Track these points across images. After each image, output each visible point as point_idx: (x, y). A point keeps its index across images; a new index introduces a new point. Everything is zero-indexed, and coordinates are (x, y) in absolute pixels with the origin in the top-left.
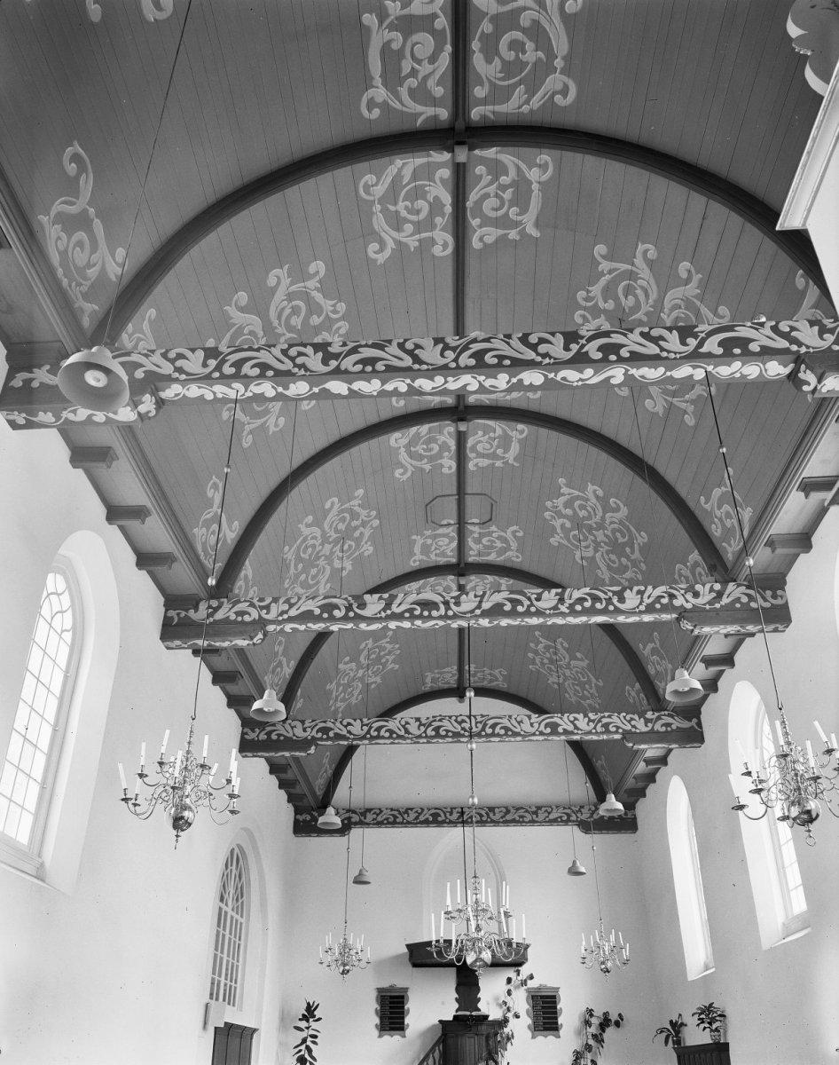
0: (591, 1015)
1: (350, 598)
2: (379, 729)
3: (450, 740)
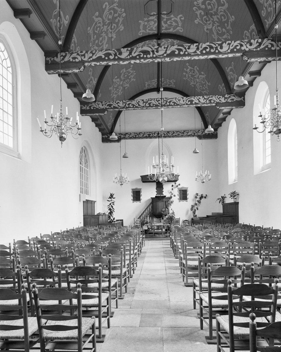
0: (197, 195)
2: (129, 104)
3: (154, 108)
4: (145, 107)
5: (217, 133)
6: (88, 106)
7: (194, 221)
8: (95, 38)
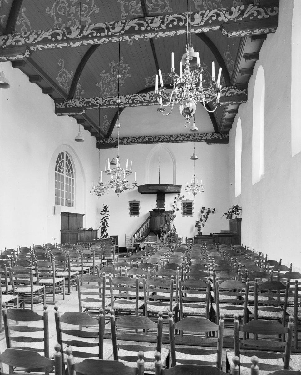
0: (204, 209)
1: (64, 29)
2: (109, 101)
3: (139, 105)
4: (128, 104)
5: (228, 136)
6: (63, 104)
7: (199, 239)
8: (60, 22)
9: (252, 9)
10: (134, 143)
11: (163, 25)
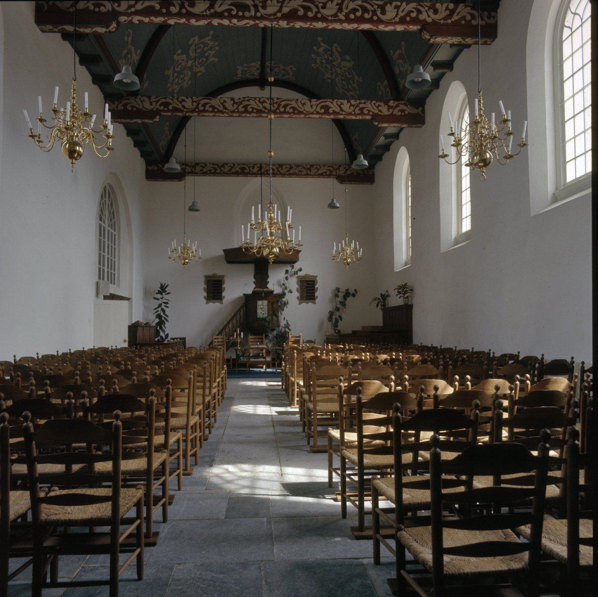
0: (339, 291)
3: (255, 115)
9: (463, 11)
10: (214, 173)
11: (341, 13)
